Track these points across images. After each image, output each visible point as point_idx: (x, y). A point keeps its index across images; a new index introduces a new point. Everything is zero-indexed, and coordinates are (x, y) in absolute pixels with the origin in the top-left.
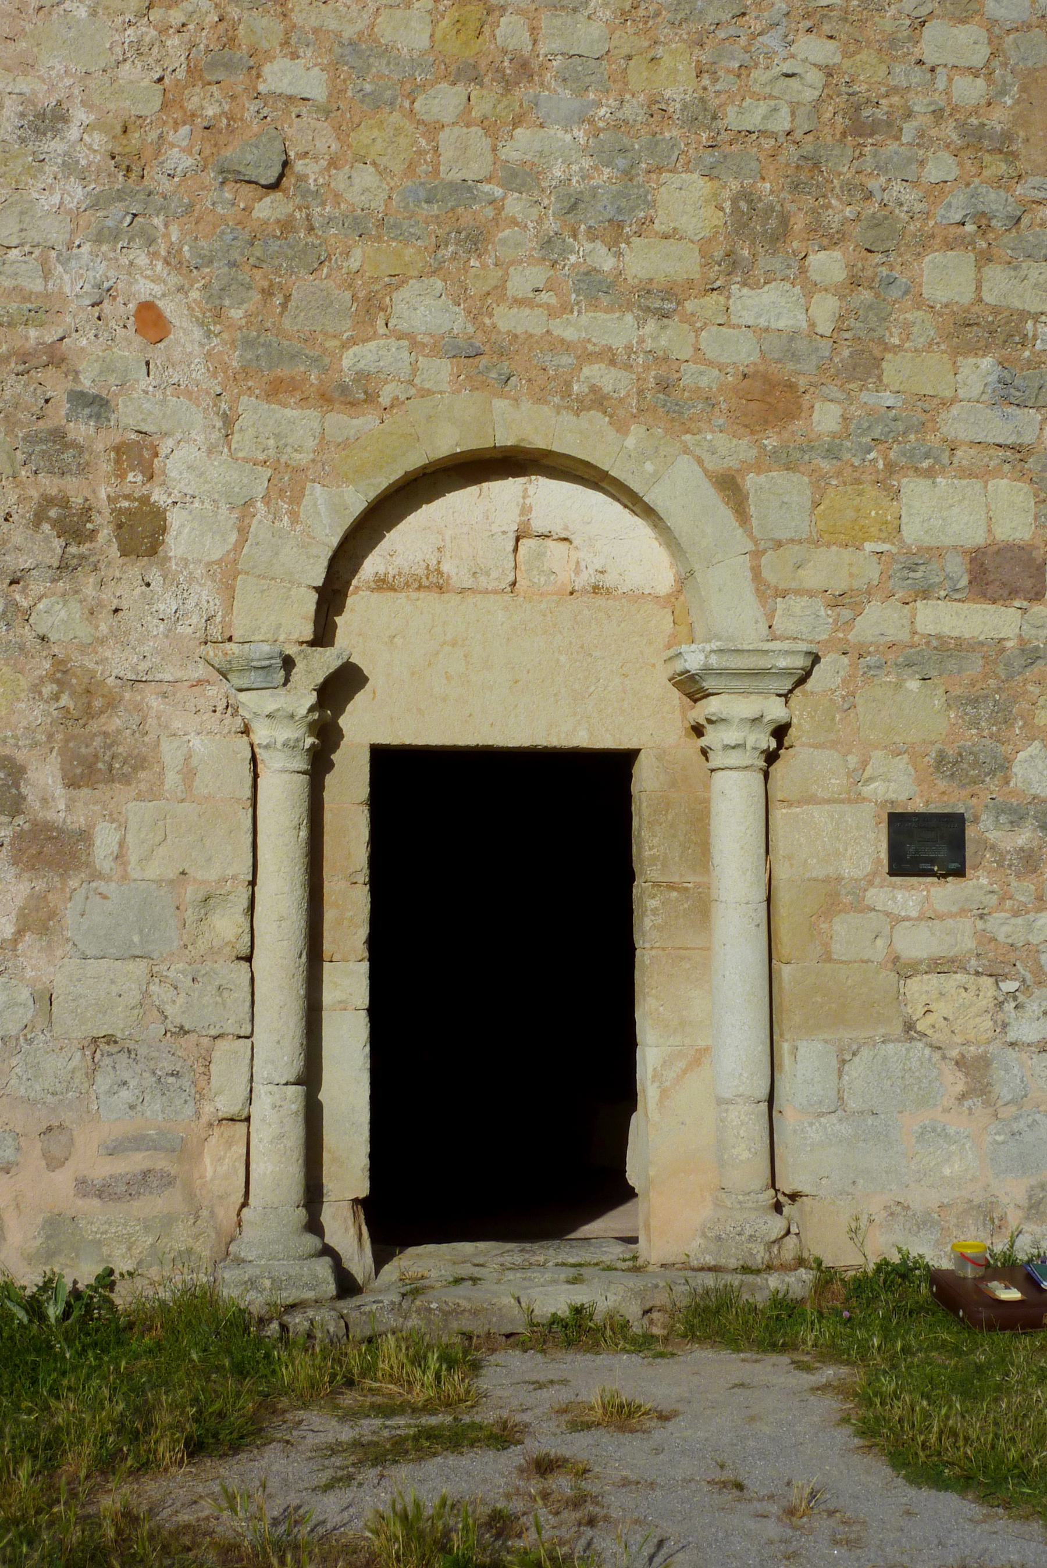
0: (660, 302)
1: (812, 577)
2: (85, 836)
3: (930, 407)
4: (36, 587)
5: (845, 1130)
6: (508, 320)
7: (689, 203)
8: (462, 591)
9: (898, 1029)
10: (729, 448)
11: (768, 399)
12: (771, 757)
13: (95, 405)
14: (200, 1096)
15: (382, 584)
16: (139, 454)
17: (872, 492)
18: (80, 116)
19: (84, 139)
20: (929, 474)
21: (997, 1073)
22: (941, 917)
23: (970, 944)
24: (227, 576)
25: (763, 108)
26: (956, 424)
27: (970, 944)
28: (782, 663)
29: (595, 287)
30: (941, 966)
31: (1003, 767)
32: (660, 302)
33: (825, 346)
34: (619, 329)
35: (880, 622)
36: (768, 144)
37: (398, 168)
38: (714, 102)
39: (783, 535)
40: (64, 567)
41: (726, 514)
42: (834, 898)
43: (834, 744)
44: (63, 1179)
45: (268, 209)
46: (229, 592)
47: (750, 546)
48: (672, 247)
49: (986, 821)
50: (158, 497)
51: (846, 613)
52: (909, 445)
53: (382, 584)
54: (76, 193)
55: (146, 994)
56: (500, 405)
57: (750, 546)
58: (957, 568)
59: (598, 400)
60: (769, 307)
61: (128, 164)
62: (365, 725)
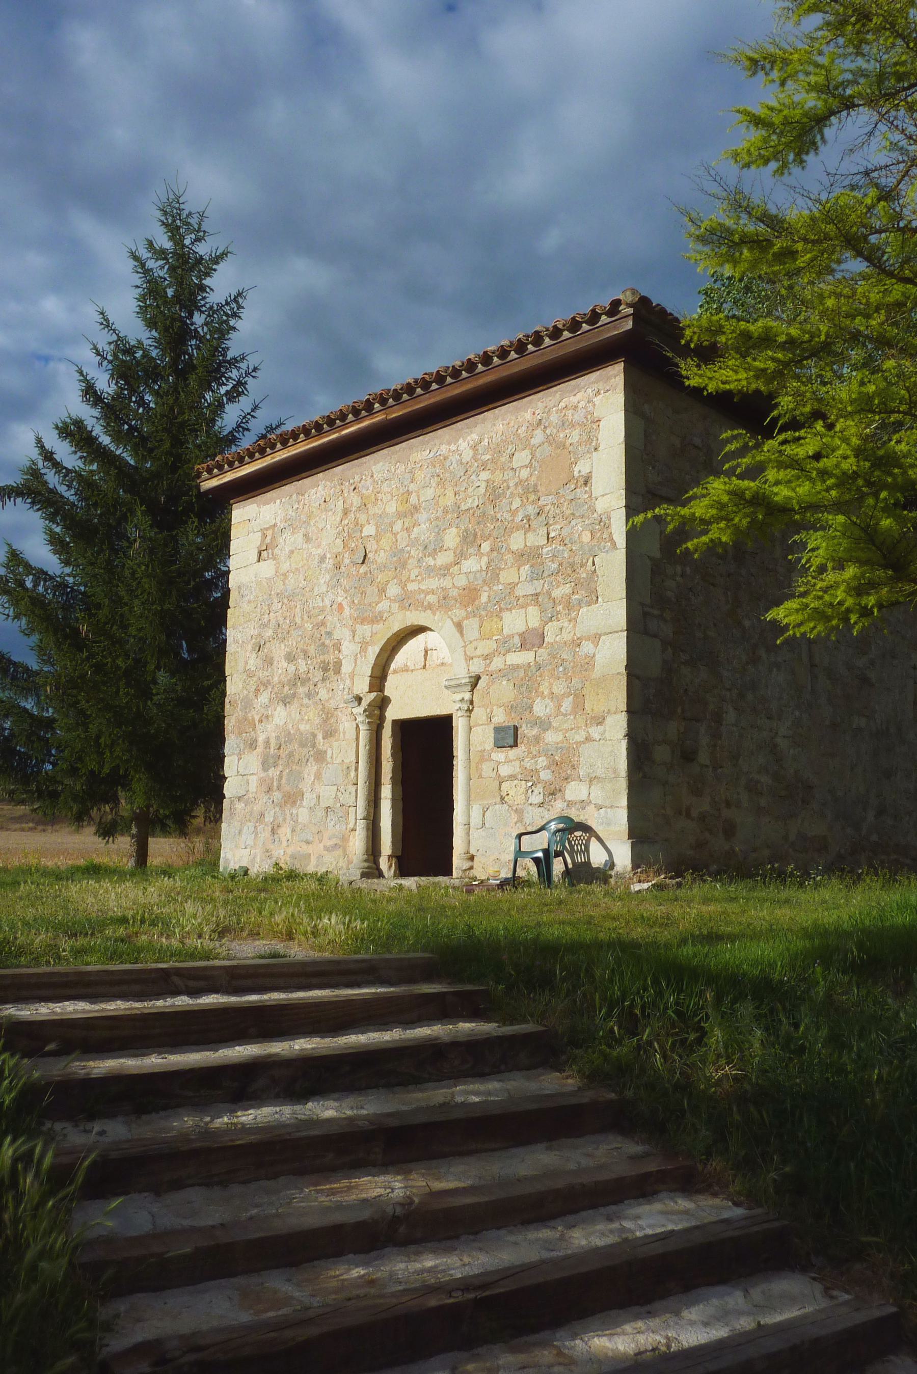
0: (444, 571)
1: (478, 652)
2: (326, 752)
3: (513, 586)
4: (319, 686)
5: (484, 834)
6: (411, 587)
7: (452, 538)
8: (412, 671)
9: (498, 799)
10: (458, 613)
11: (470, 595)
12: (470, 711)
13: (329, 634)
14: (347, 824)
15: (395, 672)
16: (338, 646)
17: (495, 619)
18: (328, 556)
19: (329, 563)
20: (510, 610)
21: (526, 815)
22: (511, 761)
23: (518, 770)
24: (352, 676)
25: (470, 500)
26: (520, 591)
27: (518, 770)
28: (463, 681)
29: (430, 570)
30: (512, 777)
31: (530, 708)
32: (444, 571)
33: (484, 573)
34: (433, 583)
35: (497, 663)
36: (471, 512)
37: (388, 549)
38: (458, 503)
39: (471, 639)
40: (324, 680)
41: (458, 635)
42: (484, 757)
43: (483, 706)
44: (321, 845)
45: (363, 569)
46: (352, 680)
47: (463, 644)
48: (447, 553)
49: (524, 726)
50: (341, 657)
51: (488, 661)
52: (509, 600)
53: (395, 672)
54: (328, 577)
55: (336, 795)
56: (408, 613)
57: (463, 644)
58: (517, 640)
59: (430, 607)
60: (471, 564)
61: (338, 567)
62: (393, 713)
